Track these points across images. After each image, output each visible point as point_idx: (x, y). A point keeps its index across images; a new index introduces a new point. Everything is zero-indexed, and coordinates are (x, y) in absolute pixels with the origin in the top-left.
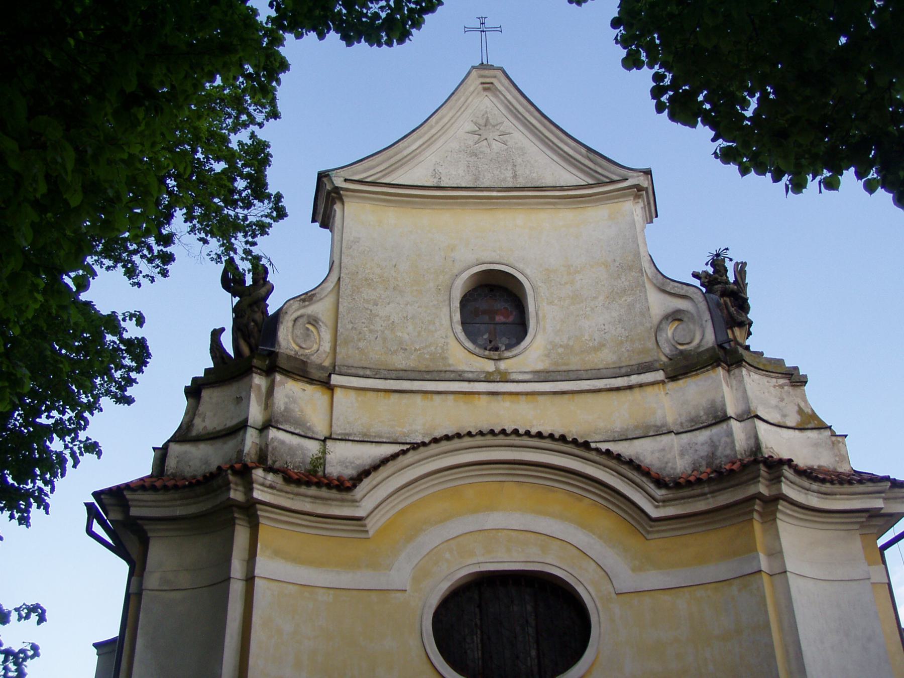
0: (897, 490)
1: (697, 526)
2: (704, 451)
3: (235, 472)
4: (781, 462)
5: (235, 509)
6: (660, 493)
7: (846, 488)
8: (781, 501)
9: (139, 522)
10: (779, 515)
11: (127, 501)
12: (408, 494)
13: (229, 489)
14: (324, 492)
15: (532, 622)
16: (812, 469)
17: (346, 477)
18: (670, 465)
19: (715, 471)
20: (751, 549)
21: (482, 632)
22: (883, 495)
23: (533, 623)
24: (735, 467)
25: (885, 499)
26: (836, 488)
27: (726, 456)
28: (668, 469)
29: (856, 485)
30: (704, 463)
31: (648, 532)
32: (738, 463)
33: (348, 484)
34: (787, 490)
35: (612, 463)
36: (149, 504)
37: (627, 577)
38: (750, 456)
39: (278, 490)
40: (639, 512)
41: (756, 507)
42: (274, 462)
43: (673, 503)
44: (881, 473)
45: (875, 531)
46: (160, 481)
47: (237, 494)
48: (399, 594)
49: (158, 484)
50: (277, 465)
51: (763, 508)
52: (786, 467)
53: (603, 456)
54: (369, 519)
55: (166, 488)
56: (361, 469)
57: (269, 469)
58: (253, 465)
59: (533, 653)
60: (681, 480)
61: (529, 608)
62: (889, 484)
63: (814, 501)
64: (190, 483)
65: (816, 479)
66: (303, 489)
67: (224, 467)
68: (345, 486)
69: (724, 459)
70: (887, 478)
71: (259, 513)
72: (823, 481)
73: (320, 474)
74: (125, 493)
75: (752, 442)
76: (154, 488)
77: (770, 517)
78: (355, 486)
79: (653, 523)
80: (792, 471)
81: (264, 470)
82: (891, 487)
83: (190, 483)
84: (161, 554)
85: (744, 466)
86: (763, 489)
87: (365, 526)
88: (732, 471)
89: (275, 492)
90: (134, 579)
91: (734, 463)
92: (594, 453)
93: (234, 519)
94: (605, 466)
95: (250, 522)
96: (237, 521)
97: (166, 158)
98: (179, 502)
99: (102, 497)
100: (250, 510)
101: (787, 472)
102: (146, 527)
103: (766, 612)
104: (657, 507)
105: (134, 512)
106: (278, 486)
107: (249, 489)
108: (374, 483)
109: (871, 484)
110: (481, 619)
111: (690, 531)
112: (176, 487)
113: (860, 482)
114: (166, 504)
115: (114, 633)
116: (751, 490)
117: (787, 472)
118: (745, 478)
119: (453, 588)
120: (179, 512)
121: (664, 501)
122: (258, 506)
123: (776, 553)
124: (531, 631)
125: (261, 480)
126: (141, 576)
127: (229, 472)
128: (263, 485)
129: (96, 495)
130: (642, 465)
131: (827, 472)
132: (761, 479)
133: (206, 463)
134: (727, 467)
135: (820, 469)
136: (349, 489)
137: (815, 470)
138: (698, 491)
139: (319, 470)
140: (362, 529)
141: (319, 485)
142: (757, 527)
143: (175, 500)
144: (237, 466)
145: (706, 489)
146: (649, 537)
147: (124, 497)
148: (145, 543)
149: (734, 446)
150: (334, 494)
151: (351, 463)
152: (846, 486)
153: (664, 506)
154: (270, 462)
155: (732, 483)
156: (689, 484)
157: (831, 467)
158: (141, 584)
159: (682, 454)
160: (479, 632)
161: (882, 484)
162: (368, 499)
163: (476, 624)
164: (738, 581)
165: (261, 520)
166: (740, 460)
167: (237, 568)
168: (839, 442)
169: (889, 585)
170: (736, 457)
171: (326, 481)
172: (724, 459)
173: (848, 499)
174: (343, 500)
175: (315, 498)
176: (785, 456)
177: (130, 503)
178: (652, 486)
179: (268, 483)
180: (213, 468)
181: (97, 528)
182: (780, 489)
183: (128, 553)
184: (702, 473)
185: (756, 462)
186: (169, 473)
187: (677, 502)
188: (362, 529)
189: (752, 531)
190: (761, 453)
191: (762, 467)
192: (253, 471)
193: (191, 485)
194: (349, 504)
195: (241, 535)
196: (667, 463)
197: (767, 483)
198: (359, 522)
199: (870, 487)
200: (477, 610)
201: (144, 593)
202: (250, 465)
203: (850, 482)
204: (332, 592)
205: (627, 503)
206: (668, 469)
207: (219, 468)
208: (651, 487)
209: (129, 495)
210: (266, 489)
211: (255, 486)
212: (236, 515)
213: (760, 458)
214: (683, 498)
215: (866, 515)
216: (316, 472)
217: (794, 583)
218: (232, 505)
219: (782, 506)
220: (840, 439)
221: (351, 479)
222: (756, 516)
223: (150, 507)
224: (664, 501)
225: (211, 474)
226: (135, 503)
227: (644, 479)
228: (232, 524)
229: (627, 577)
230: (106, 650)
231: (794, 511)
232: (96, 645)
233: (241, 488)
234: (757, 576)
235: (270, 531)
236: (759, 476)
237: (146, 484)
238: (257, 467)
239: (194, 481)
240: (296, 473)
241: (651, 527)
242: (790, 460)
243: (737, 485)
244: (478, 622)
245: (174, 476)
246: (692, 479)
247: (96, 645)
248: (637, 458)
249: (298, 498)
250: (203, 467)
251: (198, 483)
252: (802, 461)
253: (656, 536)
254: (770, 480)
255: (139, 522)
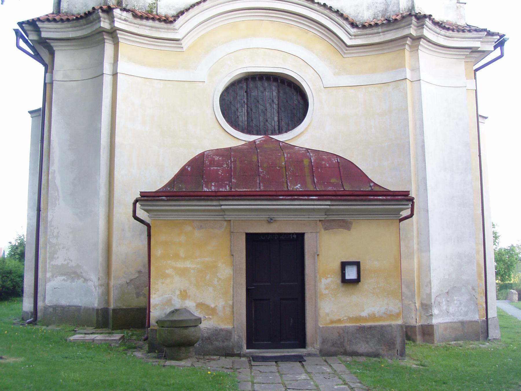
0: (490, 37)
1: (374, 51)
2: (381, 7)
3: (104, 11)
4: (425, 16)
5: (104, 33)
6: (353, 31)
7: (461, 34)
8: (422, 40)
9: (47, 41)
10: (420, 47)
11: (39, 28)
12: (206, 26)
13: (100, 21)
14: (157, 24)
15: (276, 101)
16: (443, 22)
17: (170, 16)
18: (360, 14)
19: (386, 20)
20: (403, 66)
21: (247, 106)
22: (481, 39)
23: (277, 102)
24: (397, 18)
25: (482, 42)
26: (455, 34)
27: (394, 11)
28: (359, 17)
29: (467, 33)
30: (380, 15)
31: (345, 53)
32: (400, 15)
33: (172, 19)
34: (426, 33)
35: (327, 12)
36: (53, 30)
37: (331, 78)
38: (408, 12)
39: (129, 22)
40: (341, 42)
41: (408, 42)
42: (127, 5)
43: (360, 37)
44: (481, 27)
45: (473, 60)
46: (58, 16)
47: (105, 24)
48: (201, 84)
49: (57, 18)
50: (128, 8)
51: (412, 43)
52: (427, 19)
53: (322, 7)
54: (183, 40)
55: (62, 20)
56: (179, 11)
57: (125, 10)
58: (114, 7)
59: (276, 119)
60: (366, 24)
61: (275, 94)
62: (486, 33)
63: (441, 41)
64: (77, 17)
65: (444, 28)
66: (144, 22)
67: (96, 8)
68: (167, 20)
69: (392, 13)
70: (485, 30)
71: (119, 36)
72: (448, 29)
73: (155, 13)
74: (37, 23)
75: (410, 4)
76: (55, 20)
77: (415, 48)
78: (175, 20)
79: (347, 48)
80: (431, 22)
81: (121, 10)
82: (486, 35)
83: (77, 17)
84: (63, 59)
85: (403, 18)
86: (413, 31)
87: (181, 44)
88: (396, 20)
89: (128, 23)
90: (47, 74)
91: (397, 16)
92: (316, 5)
93: (104, 39)
94: (322, 13)
95: (113, 41)
96: (106, 41)
97: (310, 385)
98: (70, 29)
99: (24, 25)
100: (113, 33)
101: (428, 22)
102: (52, 44)
103: (407, 101)
104: (351, 39)
105: (44, 35)
106: (130, 20)
107: (112, 21)
108: (187, 19)
109: (475, 33)
110: (247, 99)
111: (368, 54)
112: (68, 20)
113: (469, 31)
114: (62, 30)
115: (40, 106)
116: (406, 32)
117: (428, 22)
118: (403, 24)
119: (232, 81)
120: (71, 35)
121: (355, 36)
122: (118, 31)
123: (416, 69)
124: (275, 106)
125: (119, 16)
126: (52, 73)
127: (100, 10)
128: (120, 19)
129: (20, 24)
130: (344, 14)
131: (451, 24)
132: (412, 26)
133: (86, 6)
134: (394, 18)
135: (447, 23)
136: (171, 22)
137: (444, 22)
138: (375, 30)
139: (154, 10)
140: (180, 46)
141: (153, 19)
142: (407, 53)
143: (68, 28)
144: (105, 7)
145: (380, 30)
146: (345, 56)
147: (37, 25)
148: (52, 53)
149: (399, 5)
150: (163, 25)
151: (173, 7)
152: (461, 33)
153: (355, 39)
154: (124, 5)
155: (395, 27)
156: (370, 26)
157: (454, 22)
158: (52, 77)
159: (368, 9)
160: (246, 106)
161: (480, 33)
162: (182, 28)
163: (244, 102)
164: (393, 83)
165: (120, 40)
166: (402, 14)
167: (107, 68)
168: (461, 7)
169: (476, 91)
170: (399, 12)
171: (158, 17)
172: (392, 13)
173: (460, 41)
174: (168, 29)
175: (152, 27)
176: (428, 13)
177: (41, 29)
178: (349, 26)
179: (123, 18)
180: (90, 9)
181: (22, 44)
182: (423, 33)
183: (42, 59)
184: (378, 20)
185: (410, 15)
186: (63, 12)
187: (363, 36)
188: (180, 46)
189: (404, 56)
190: (414, 10)
191: (413, 18)
192: (114, 10)
193: (77, 19)
194: (172, 31)
195: (109, 48)
196: (359, 13)
197: (415, 28)
198: (177, 42)
199: (474, 34)
200: (245, 94)
201: (54, 82)
202: (112, 7)
203: (463, 31)
204: (162, 82)
205: (333, 35)
206: (359, 17)
207: (94, 8)
208: (348, 27)
209: (39, 24)
210: (122, 21)
211: (115, 19)
212: (105, 37)
213: (413, 13)
214: (366, 34)
215: (470, 51)
216: (152, 12)
217: (424, 86)
218: (101, 32)
219: (422, 42)
220: (461, 5)
221: (173, 16)
222: (407, 47)
223: (53, 32)
224: (355, 36)
225: (89, 12)
226: (44, 29)
227: (345, 22)
228: (103, 42)
229: (331, 78)
230: (35, 115)
231: (430, 46)
232: (31, 112)
233: (107, 21)
234: (404, 81)
235: (125, 45)
236: (411, 24)
237: (50, 18)
238: (116, 8)
239: (79, 16)
240: (140, 12)
241: (346, 50)
242: (430, 16)
243: (398, 28)
244: (246, 101)
245: (67, 14)
246: (372, 23)
247: (31, 112)
248: (342, 10)
249: (141, 27)
250: (84, 8)
251: (82, 17)
252: (437, 18)
253: (349, 56)
254: (418, 27)
255: (47, 41)
